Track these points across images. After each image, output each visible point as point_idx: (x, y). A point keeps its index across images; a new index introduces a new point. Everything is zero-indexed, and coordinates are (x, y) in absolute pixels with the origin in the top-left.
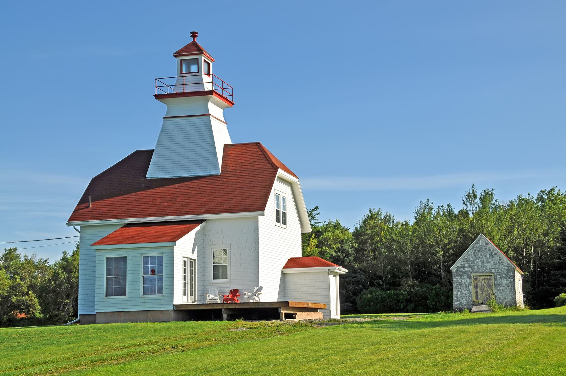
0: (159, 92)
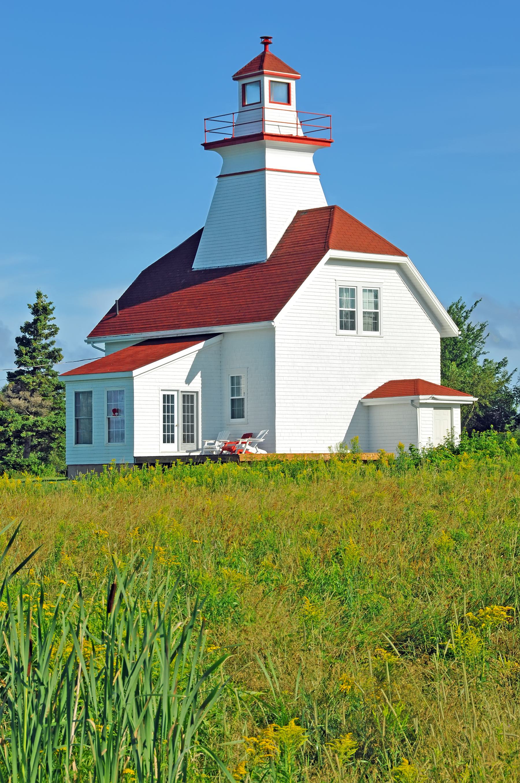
0: (212, 138)
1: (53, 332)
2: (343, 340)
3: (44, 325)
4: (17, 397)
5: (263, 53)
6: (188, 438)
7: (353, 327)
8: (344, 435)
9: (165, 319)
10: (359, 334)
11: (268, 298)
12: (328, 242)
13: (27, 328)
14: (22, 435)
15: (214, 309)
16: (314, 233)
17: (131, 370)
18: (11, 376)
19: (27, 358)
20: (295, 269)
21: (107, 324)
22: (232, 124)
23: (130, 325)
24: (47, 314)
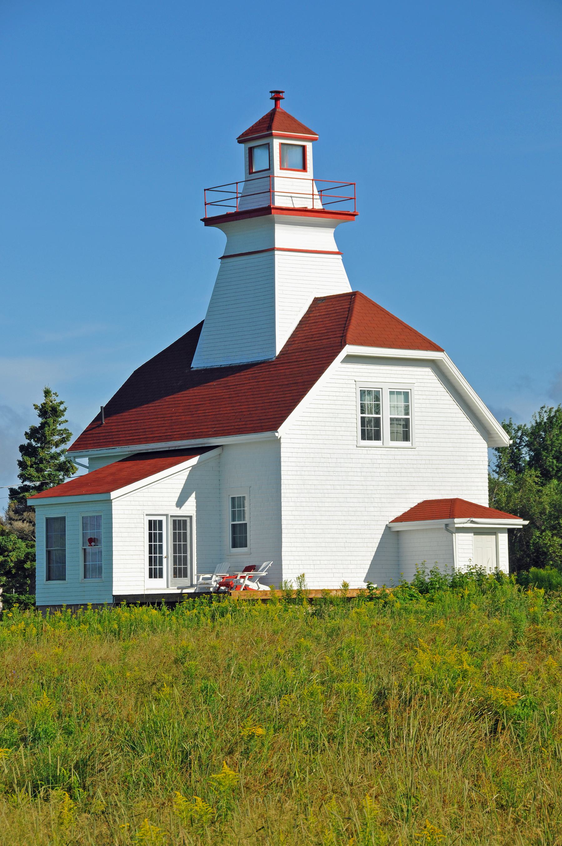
1: (64, 438)
2: (365, 452)
3: (53, 430)
4: (20, 520)
5: (272, 110)
6: (180, 572)
7: (377, 437)
8: (368, 567)
9: (156, 429)
10: (385, 445)
11: (273, 403)
12: (345, 336)
13: (33, 433)
14: (26, 566)
15: (212, 416)
16: (331, 324)
17: (109, 491)
18: (13, 493)
19: (32, 471)
20: (306, 368)
21: (91, 436)
22: (235, 195)
23: (116, 436)
24: (57, 416)
